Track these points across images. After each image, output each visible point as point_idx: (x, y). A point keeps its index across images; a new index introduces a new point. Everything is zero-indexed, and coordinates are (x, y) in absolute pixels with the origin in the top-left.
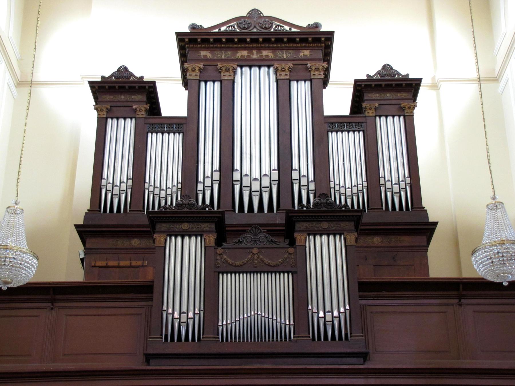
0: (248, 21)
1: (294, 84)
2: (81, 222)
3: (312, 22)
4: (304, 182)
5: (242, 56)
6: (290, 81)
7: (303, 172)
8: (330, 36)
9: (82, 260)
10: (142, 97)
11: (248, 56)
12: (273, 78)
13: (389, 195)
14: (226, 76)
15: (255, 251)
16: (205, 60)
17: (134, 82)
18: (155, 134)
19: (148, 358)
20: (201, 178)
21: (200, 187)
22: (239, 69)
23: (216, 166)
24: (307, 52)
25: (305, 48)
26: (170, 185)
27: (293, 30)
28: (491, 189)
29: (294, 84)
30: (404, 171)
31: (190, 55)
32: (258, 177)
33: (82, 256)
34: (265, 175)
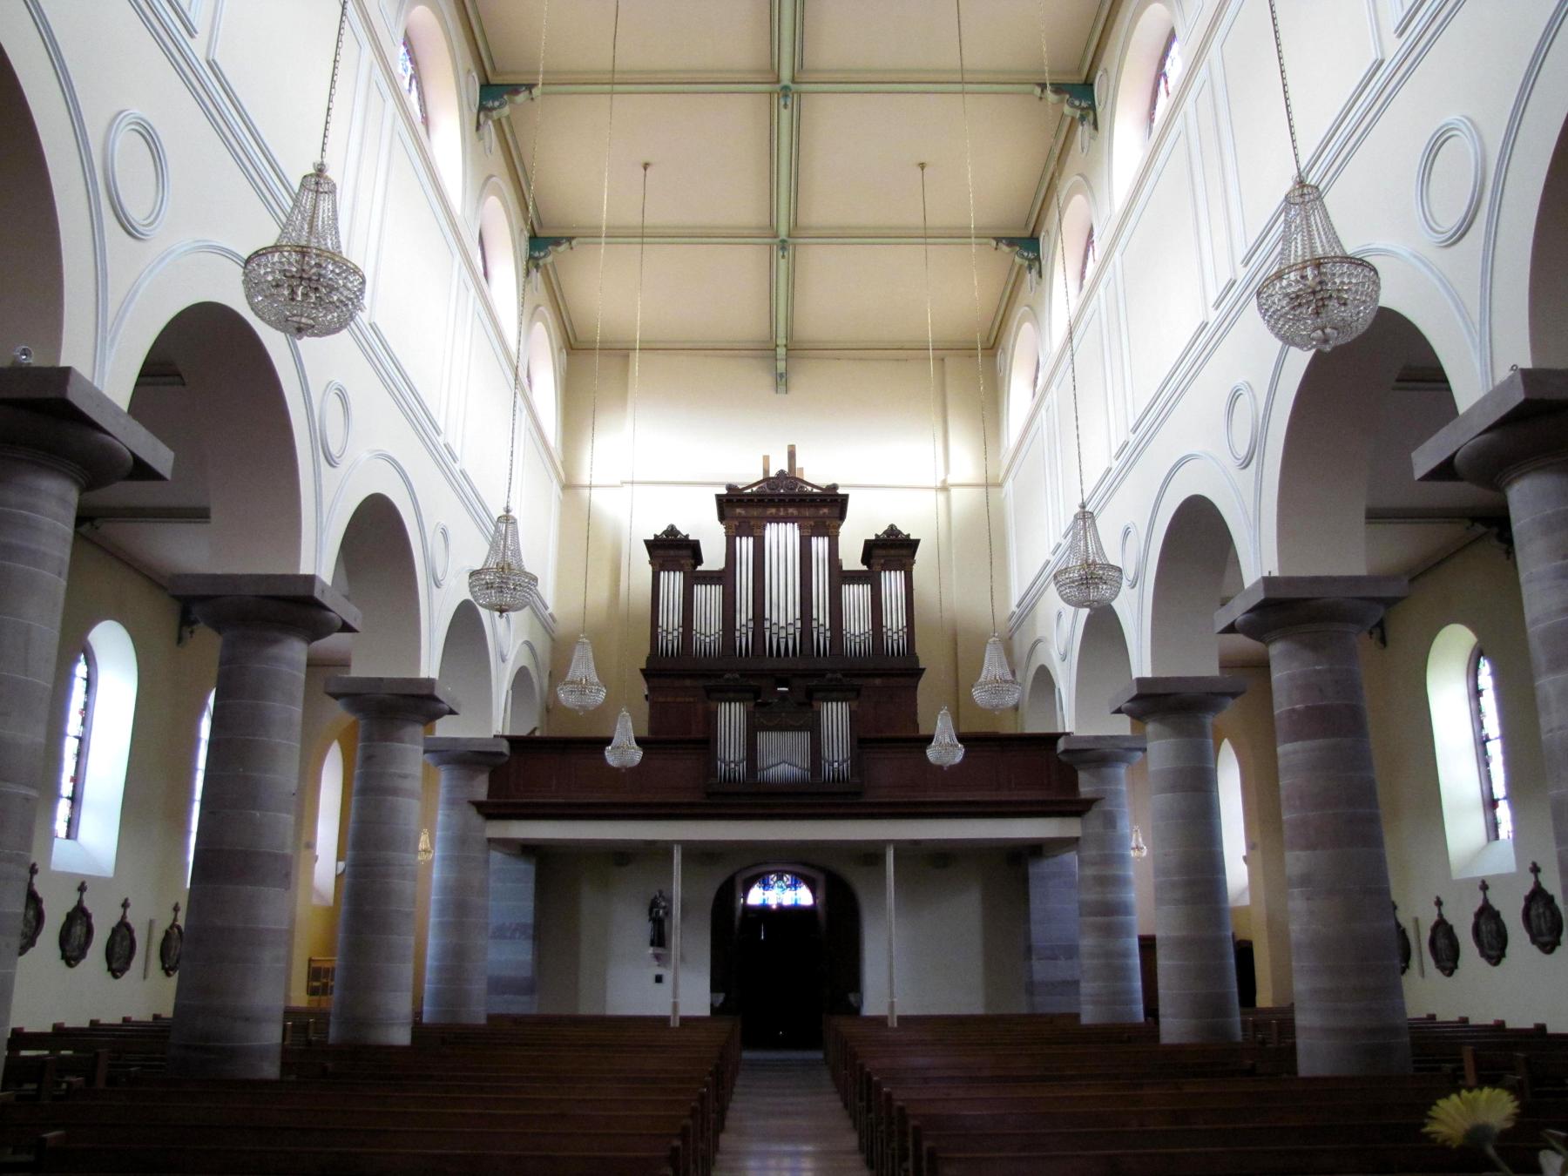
0: (777, 482)
1: (814, 540)
2: (644, 667)
3: (830, 483)
4: (822, 629)
5: (771, 514)
6: (811, 536)
7: (821, 622)
8: (845, 498)
9: (646, 696)
10: (688, 552)
11: (776, 514)
12: (797, 533)
13: (890, 641)
14: (757, 532)
15: (783, 714)
16: (739, 517)
17: (680, 540)
18: (699, 586)
19: (709, 795)
20: (738, 627)
21: (737, 634)
22: (768, 524)
23: (750, 616)
24: (826, 510)
25: (825, 507)
26: (713, 632)
27: (815, 490)
28: (1297, 141)
29: (814, 540)
30: (902, 622)
31: (727, 511)
32: (784, 625)
33: (646, 693)
34: (790, 624)
